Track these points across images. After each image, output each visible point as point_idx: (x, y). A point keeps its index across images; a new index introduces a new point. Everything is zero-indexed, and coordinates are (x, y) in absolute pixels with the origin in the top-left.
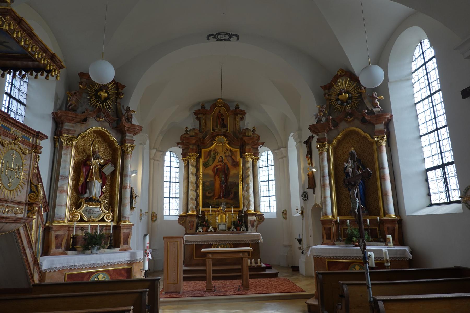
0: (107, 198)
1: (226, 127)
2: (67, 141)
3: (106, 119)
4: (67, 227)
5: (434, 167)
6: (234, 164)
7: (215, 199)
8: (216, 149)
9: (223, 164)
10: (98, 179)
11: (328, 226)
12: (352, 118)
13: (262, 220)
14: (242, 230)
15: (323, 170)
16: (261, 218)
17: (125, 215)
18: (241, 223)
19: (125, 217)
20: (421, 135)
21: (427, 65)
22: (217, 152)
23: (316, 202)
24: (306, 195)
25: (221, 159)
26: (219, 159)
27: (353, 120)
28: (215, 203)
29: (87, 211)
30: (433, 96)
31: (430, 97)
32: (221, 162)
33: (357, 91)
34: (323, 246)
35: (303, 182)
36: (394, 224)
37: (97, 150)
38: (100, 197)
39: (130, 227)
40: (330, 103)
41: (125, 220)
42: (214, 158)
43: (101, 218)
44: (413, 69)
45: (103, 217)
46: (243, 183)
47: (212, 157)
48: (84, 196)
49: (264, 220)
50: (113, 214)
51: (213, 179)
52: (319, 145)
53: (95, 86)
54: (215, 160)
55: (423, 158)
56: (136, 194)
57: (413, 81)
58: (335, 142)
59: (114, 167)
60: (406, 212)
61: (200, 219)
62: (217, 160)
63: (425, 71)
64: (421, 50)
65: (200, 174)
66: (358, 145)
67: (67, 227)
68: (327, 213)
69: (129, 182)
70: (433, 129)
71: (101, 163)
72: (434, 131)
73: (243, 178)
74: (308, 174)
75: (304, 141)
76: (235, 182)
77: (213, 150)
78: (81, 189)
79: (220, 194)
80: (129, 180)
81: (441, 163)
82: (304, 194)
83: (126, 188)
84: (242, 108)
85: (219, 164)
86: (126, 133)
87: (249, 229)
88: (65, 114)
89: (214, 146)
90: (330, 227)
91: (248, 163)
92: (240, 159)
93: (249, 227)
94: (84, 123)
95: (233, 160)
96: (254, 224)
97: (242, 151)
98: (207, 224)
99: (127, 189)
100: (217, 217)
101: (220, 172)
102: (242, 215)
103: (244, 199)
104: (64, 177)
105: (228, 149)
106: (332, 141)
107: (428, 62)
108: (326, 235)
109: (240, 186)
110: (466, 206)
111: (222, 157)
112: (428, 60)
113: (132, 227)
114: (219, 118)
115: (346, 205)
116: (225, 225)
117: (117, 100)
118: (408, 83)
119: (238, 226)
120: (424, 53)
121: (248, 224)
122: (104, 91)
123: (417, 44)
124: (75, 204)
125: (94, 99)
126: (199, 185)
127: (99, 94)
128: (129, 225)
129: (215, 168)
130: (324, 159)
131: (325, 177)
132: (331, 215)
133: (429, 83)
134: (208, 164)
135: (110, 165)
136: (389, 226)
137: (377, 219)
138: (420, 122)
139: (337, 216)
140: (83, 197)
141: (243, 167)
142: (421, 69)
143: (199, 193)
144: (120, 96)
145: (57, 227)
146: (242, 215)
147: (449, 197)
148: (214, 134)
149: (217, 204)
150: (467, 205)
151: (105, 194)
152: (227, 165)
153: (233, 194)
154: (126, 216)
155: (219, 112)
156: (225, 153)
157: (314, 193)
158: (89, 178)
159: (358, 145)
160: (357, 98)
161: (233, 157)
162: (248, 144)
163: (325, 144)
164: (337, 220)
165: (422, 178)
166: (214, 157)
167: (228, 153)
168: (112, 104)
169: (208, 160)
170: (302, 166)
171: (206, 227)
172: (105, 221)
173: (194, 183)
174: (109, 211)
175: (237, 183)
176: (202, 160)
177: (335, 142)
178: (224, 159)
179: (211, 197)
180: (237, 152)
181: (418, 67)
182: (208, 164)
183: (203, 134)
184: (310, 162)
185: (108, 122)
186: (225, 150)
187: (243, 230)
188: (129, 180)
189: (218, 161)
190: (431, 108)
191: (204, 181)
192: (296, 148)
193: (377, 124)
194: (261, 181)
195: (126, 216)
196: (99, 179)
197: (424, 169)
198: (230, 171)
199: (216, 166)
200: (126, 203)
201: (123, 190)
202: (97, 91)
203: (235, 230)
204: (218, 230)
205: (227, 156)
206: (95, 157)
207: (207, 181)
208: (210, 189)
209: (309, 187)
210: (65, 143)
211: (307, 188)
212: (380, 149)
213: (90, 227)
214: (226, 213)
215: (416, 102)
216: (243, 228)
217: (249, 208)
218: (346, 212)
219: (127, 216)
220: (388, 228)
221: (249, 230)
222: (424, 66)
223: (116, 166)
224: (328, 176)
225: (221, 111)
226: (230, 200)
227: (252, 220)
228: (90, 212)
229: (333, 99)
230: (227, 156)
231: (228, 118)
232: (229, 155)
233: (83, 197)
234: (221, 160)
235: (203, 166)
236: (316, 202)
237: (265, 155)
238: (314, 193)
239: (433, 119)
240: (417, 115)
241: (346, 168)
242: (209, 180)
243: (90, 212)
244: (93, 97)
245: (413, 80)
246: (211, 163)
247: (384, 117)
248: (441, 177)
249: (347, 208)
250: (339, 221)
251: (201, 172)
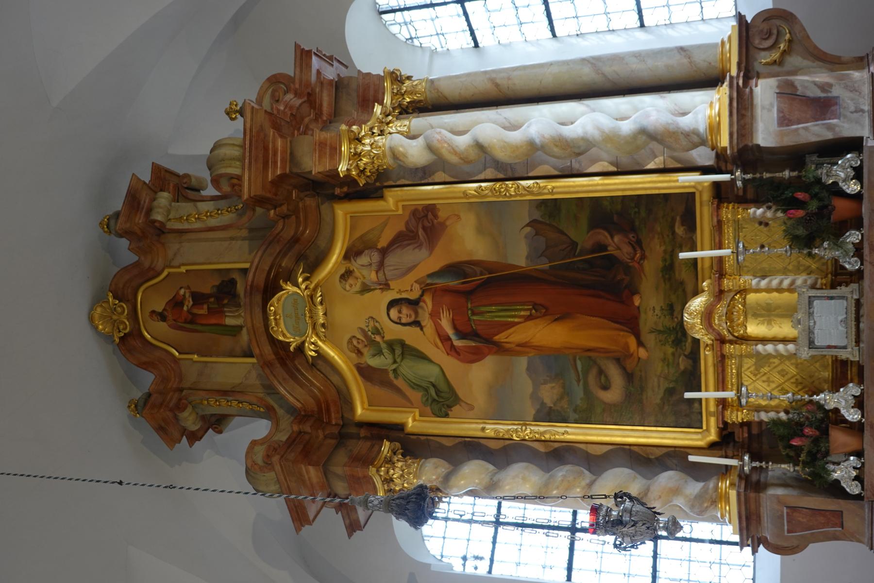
1: (233, 282)
6: (421, 232)
7: (642, 353)
8: (350, 341)
9: (428, 302)
13: (778, 22)
14: (853, 187)
16: (770, 34)
18: (800, 195)
22: (363, 331)
25: (400, 312)
26: (404, 325)
28: (670, 350)
32: (417, 313)
34: (643, 178)
42: (398, 351)
46: (530, 174)
47: (395, 362)
49: (785, 11)
51: (522, 362)
54: (409, 347)
62: (410, 336)
65: (492, 434)
73: (501, 176)
76: (528, 225)
77: (354, 355)
79: (614, 319)
84: (118, 204)
85: (427, 322)
87: (847, 129)
89: (332, 353)
91: (405, 155)
92: (391, 201)
93: (829, 136)
95: (403, 239)
96: (810, 94)
97: (345, 189)
98: (807, 431)
100: (760, 347)
101: (475, 318)
102: (739, 184)
103: (637, 168)
105: (343, 271)
109: (552, 193)
111: (392, 304)
114: (193, 319)
116: (816, 303)
119: (824, 211)
121: (814, 139)
126: (556, 445)
129: (452, 347)
134: (434, 386)
141: (440, 176)
143: (611, 447)
146: (739, 184)
148: (268, 350)
149: (673, 337)
152: (431, 276)
153: (603, 236)
155: (162, 317)
156: (366, 289)
161: (383, 243)
162: (292, 158)
166: (393, 351)
167: (365, 272)
169: (415, 386)
171: (825, 433)
173: (548, 475)
175: (537, 215)
176: (412, 422)
178: (400, 292)
179: (629, 377)
180: (354, 221)
182: (434, 386)
183: (276, 406)
186: (348, 287)
187: (852, 173)
189: (416, 330)
191: (533, 412)
194: (550, 35)
198: (464, 258)
199: (445, 339)
203: (853, 237)
204: (850, 354)
205: (381, 274)
207: (534, 396)
208: (578, 381)
214: (730, 291)
216: (842, 175)
217: (695, 132)
221: (856, 133)
225: (159, 309)
226: (643, 257)
227: (780, 111)
230: (381, 274)
231: (183, 269)
232: (374, 267)
234: (405, 310)
235: (446, 415)
237: (406, 23)
242: (525, 384)
246: (429, 372)
251: (483, 429)
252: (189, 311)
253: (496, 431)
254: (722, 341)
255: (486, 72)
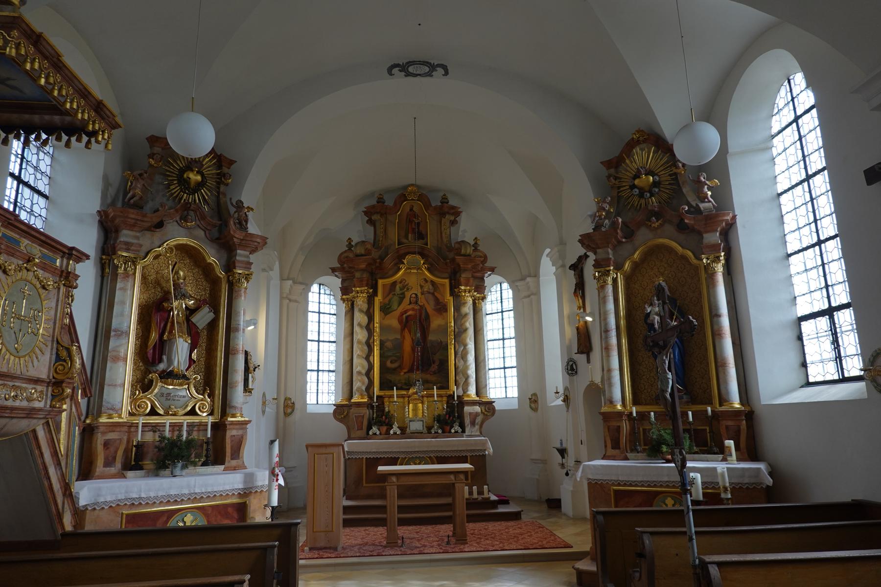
0: (201, 372)
1: (423, 239)
2: (125, 264)
3: (198, 223)
4: (125, 426)
5: (813, 313)
6: (439, 307)
7: (402, 374)
8: (404, 280)
9: (417, 307)
10: (184, 336)
11: (614, 424)
12: (660, 222)
13: (492, 412)
14: (453, 431)
15: (605, 319)
16: (489, 410)
17: (234, 404)
19: (235, 407)
20: (789, 253)
21: (800, 121)
22: (407, 285)
23: (592, 379)
24: (574, 367)
25: (414, 298)
26: (410, 299)
27: (661, 225)
28: (403, 382)
29: (163, 396)
30: (811, 181)
31: (806, 182)
32: (414, 303)
33: (669, 171)
34: (605, 462)
35: (567, 342)
36: (739, 420)
37: (182, 281)
38: (187, 370)
39: (244, 426)
40: (619, 192)
41: (234, 412)
42: (401, 296)
43: (189, 408)
44: (774, 130)
45: (194, 407)
46: (456, 343)
47: (398, 294)
48: (158, 368)
49: (495, 413)
50: (213, 401)
51: (399, 337)
52: (599, 272)
53: (179, 162)
54: (403, 299)
55: (793, 296)
56: (255, 363)
57: (775, 152)
58: (627, 266)
59: (213, 313)
60: (761, 398)
61: (375, 411)
62: (406, 301)
63: (796, 133)
64: (789, 94)
65: (375, 326)
66: (671, 271)
67: (125, 426)
68: (614, 400)
69: (242, 342)
70: (812, 241)
71: (190, 306)
72: (813, 246)
73: (456, 333)
74: (578, 327)
75: (570, 265)
76: (441, 341)
77: (400, 280)
78: (151, 355)
79: (413, 365)
80: (241, 338)
81: (826, 306)
82: (571, 363)
83: (236, 353)
84: (453, 202)
85: (410, 307)
86: (236, 250)
87: (467, 430)
88: (121, 214)
89: (400, 273)
90: (619, 426)
92: (450, 298)
93: (466, 425)
94: (158, 230)
95: (437, 300)
97: (453, 284)
98: (387, 420)
99: (238, 354)
100: (407, 407)
101: (412, 323)
102: (454, 402)
103: (457, 373)
104: (120, 332)
105: (428, 279)
106: (623, 265)
107: (803, 117)
108: (612, 440)
109: (450, 348)
110: (874, 386)
111: (416, 295)
112: (802, 112)
113: (248, 426)
114: (411, 222)
115: (648, 384)
116: (422, 422)
117: (219, 188)
118: (766, 156)
119: (446, 423)
120: (796, 100)
122: (195, 170)
123: (781, 83)
124: (140, 382)
125: (177, 185)
126: (372, 346)
127: (185, 176)
128: (242, 421)
129: (403, 315)
130: (607, 298)
131: (609, 333)
132: (621, 404)
133: (804, 157)
134: (390, 307)
135: (206, 309)
136: (730, 423)
137: (707, 411)
138: (787, 229)
139: (631, 406)
140: (156, 369)
141: (456, 314)
142: (789, 129)
143: (372, 363)
144: (226, 179)
145: (106, 426)
146: (454, 402)
147: (842, 369)
148: (402, 252)
149: (407, 382)
150: (876, 385)
151: (197, 363)
153: (437, 363)
154: (237, 405)
155: (411, 210)
156: (422, 287)
157: (588, 361)
158: (166, 334)
159: (671, 271)
160: (670, 184)
161: (436, 294)
162: (465, 270)
163: (609, 271)
164: (631, 413)
165: (791, 334)
166: (401, 294)
167: (427, 287)
168: (209, 194)
169: (390, 301)
170: (566, 312)
172: (197, 414)
173: (364, 343)
174: (204, 396)
175: (444, 344)
176: (378, 300)
177: (627, 266)
178: (421, 298)
179: (395, 369)
180: (443, 285)
181: (783, 125)
182: (390, 307)
183: (381, 251)
184: (581, 304)
185: (203, 228)
186: (422, 281)
187: (456, 431)
188: (241, 338)
189: (408, 303)
190: (808, 202)
191: (383, 339)
192: (555, 277)
193: (707, 232)
194: (489, 339)
195: (237, 406)
196: (185, 335)
197: (794, 317)
198: (431, 320)
199: (406, 312)
200: (236, 381)
201: (230, 355)
202: (182, 171)
204: (408, 431)
205: (426, 292)
206: (178, 294)
207: (388, 340)
208: (393, 354)
209: (580, 350)
210: (123, 268)
211: (575, 353)
212: (712, 279)
213: (170, 426)
214: (423, 399)
215: (779, 192)
216: (456, 428)
217: (467, 391)
218: (649, 398)
219: (238, 405)
220: (727, 427)
221: (466, 432)
222: (794, 125)
223: (217, 312)
224: (615, 330)
226: (431, 374)
227: (473, 413)
228: (169, 398)
229: (625, 186)
230: (426, 292)
231: (428, 221)
232: (429, 290)
233: (155, 370)
234: (415, 299)
235: (380, 311)
236: (592, 379)
237: (496, 291)
238: (588, 361)
239: (812, 222)
240: (782, 216)
241: (648, 315)
242: (392, 337)
243: (169, 398)
244: (175, 182)
245: (774, 149)
246: (395, 306)
247: (720, 219)
248: (826, 331)
249: (651, 390)
250: (635, 415)
251: (377, 323)
252: (413, 220)
253: (376, 327)
254: (409, 397)
255: (483, 326)
